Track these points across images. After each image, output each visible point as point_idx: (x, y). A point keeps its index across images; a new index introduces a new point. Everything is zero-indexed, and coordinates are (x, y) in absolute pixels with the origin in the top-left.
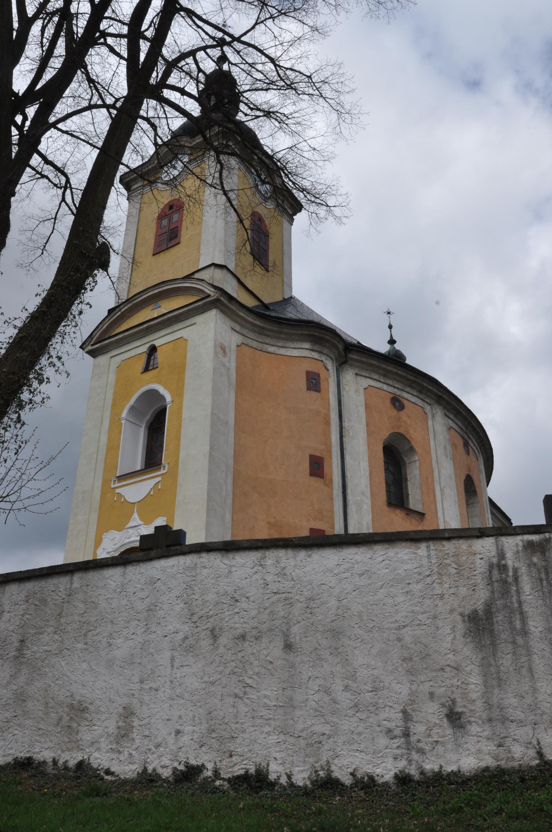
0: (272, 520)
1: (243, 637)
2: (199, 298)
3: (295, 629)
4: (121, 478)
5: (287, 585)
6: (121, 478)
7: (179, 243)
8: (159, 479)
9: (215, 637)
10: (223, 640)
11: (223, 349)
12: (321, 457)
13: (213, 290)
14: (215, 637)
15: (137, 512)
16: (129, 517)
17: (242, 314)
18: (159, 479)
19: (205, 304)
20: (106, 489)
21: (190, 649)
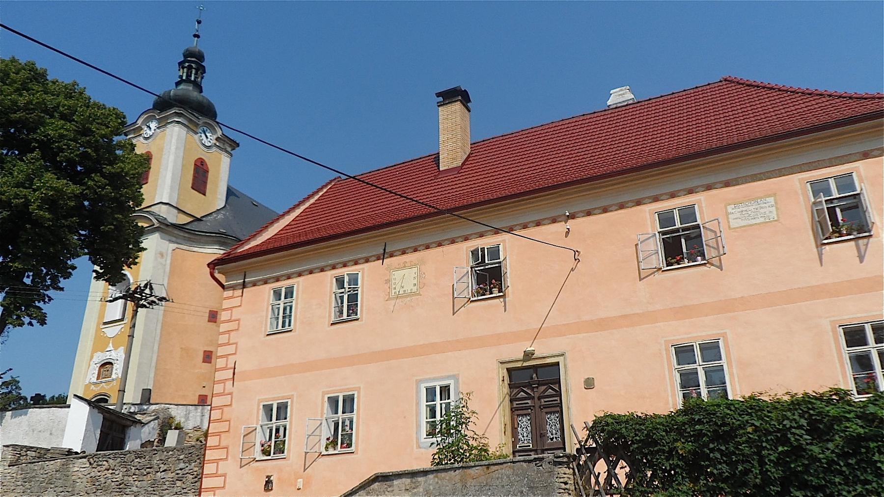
0: (183, 347)
1: (40, 431)
2: (148, 225)
3: (54, 429)
4: (105, 323)
5: (54, 417)
6: (105, 323)
7: (147, 183)
8: (123, 326)
9: (33, 431)
10: (35, 432)
11: (162, 255)
12: (209, 313)
14: (33, 431)
15: (112, 343)
16: (107, 345)
17: (176, 232)
18: (123, 326)
20: (98, 330)
21: (27, 435)
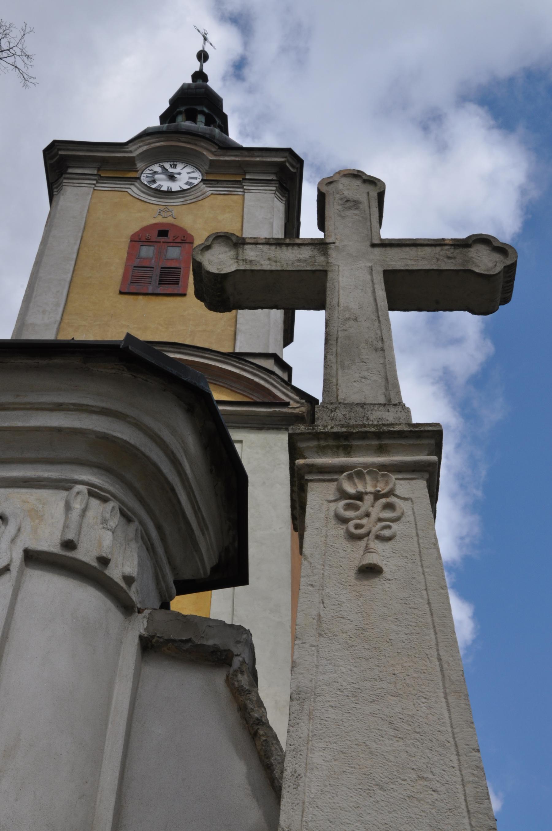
13: (297, 398)
19: (270, 415)
